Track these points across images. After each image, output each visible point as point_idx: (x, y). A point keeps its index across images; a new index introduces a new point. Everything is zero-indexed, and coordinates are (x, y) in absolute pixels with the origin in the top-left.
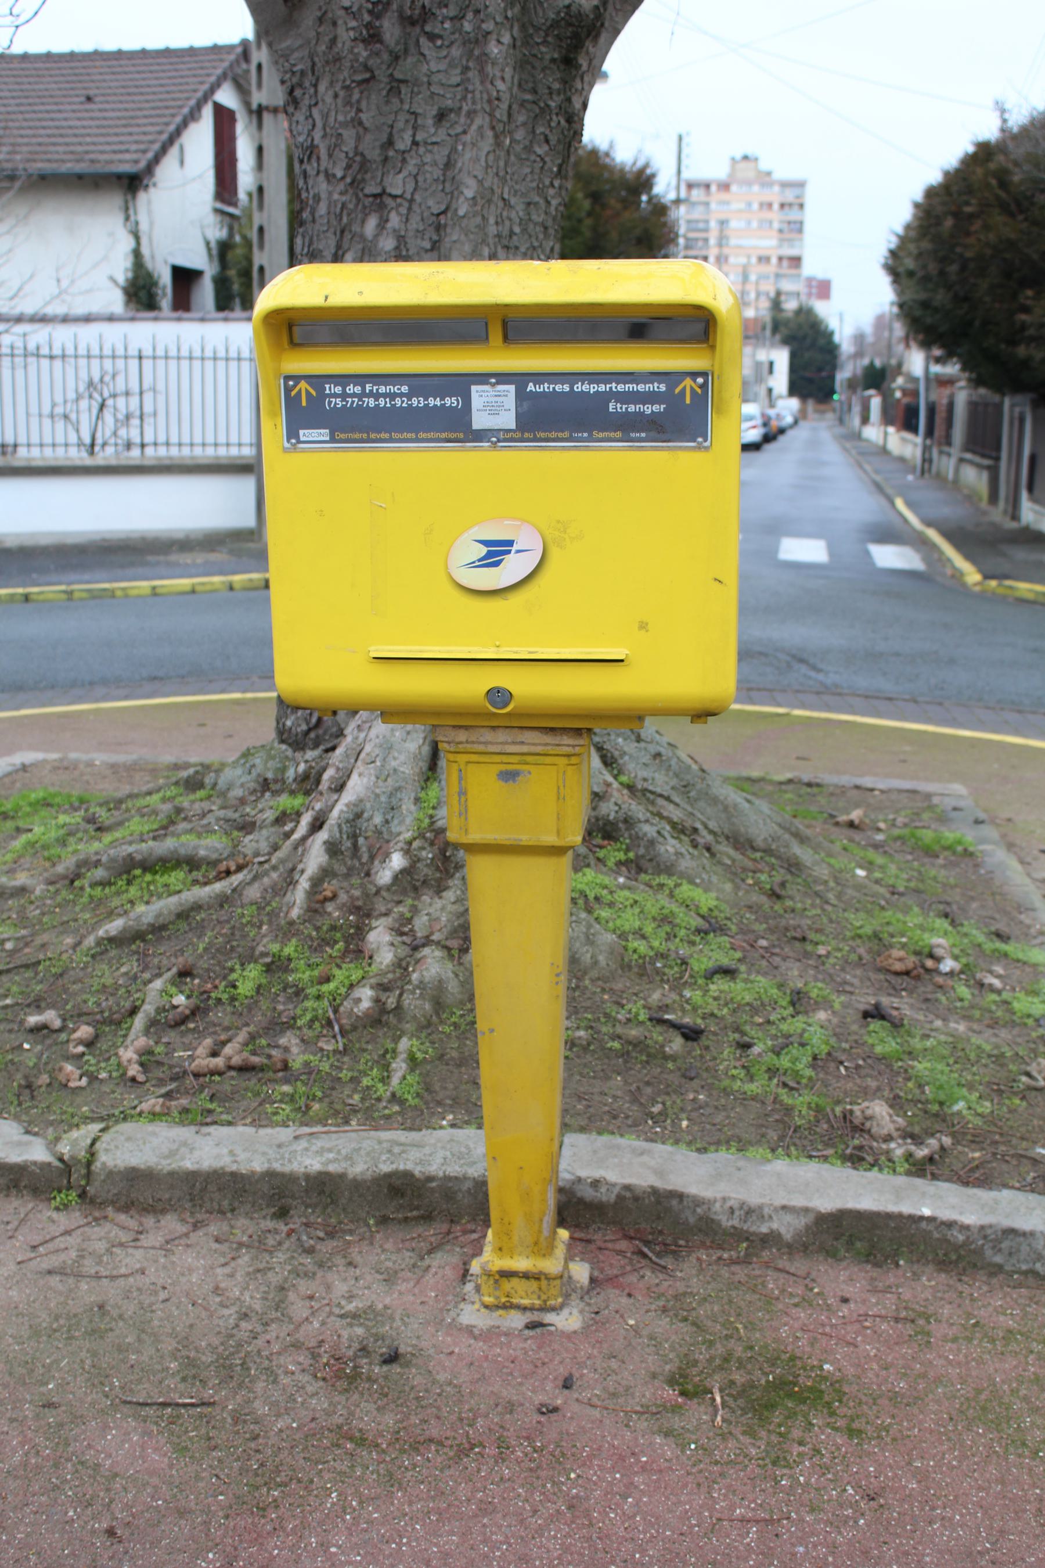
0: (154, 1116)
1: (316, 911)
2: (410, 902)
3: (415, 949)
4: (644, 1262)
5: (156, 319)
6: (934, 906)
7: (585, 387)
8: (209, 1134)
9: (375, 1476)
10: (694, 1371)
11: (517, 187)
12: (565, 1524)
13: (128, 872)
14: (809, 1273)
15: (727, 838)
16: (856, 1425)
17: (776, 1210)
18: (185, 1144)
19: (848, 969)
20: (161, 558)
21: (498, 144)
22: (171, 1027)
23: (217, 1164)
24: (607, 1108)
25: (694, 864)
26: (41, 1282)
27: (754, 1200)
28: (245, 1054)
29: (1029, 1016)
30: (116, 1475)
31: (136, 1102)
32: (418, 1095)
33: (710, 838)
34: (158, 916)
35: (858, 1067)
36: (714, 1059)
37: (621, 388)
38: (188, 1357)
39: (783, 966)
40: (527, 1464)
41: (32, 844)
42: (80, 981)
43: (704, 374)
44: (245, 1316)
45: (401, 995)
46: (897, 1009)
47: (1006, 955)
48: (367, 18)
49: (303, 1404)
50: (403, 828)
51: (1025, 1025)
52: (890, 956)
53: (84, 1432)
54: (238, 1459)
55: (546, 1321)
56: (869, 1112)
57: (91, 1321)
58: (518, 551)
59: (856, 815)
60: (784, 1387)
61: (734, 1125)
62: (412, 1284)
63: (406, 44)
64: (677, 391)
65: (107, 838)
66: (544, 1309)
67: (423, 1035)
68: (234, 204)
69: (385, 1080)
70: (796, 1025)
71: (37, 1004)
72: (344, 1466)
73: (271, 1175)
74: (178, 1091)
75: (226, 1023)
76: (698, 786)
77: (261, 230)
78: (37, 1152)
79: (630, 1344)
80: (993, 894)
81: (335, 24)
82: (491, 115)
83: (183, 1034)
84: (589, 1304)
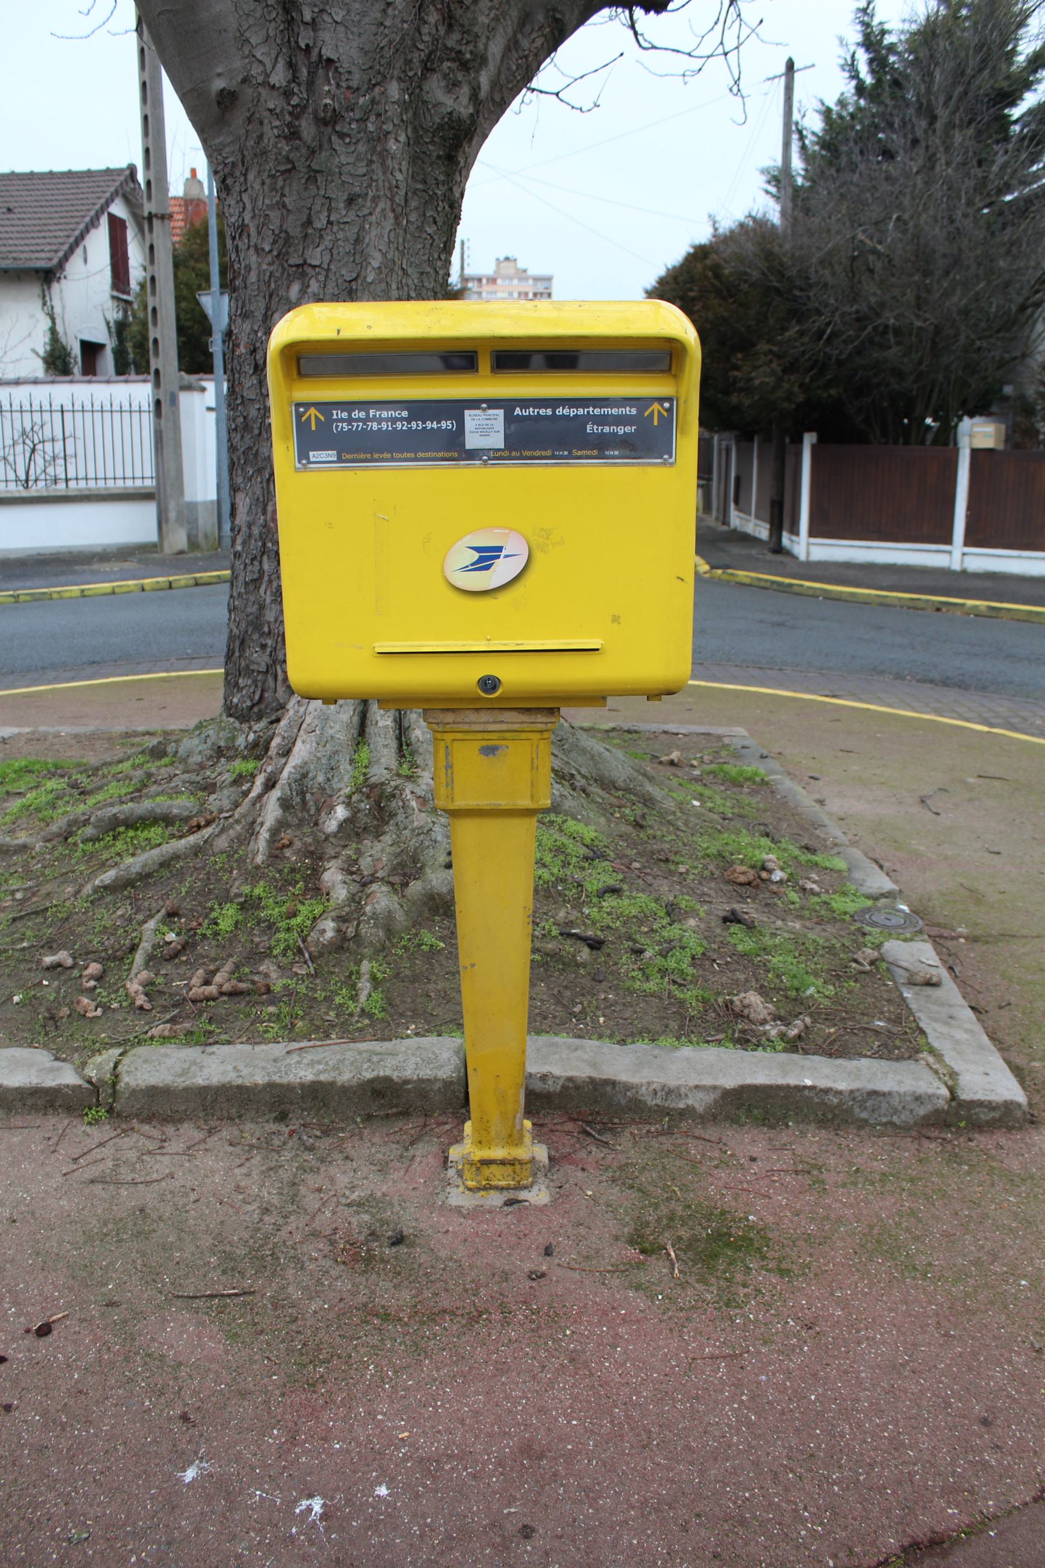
0: (164, 1039)
1: (276, 857)
2: (354, 845)
3: (364, 885)
4: (589, 1140)
5: (71, 382)
6: (756, 828)
7: (566, 411)
8: (213, 1053)
9: (403, 1347)
10: (648, 1231)
11: (412, 260)
12: (570, 1376)
13: (114, 829)
14: (720, 1139)
15: (596, 781)
16: (784, 1266)
17: (690, 1089)
18: (194, 1063)
19: (704, 883)
20: (86, 567)
21: (398, 223)
22: (166, 960)
23: (225, 1079)
24: (537, 1011)
25: (575, 803)
26: (87, 1191)
27: (673, 1083)
28: (234, 982)
29: (845, 913)
30: (180, 1364)
31: (147, 1028)
32: (384, 1010)
33: (583, 782)
34: (144, 866)
35: (727, 963)
36: (616, 964)
37: (597, 411)
38: (225, 1252)
39: (656, 883)
40: (528, 1326)
41: (27, 807)
42: (83, 923)
43: (670, 400)
44: (266, 1211)
45: (358, 925)
46: (747, 913)
47: (816, 864)
48: (288, 118)
49: (330, 1286)
50: (342, 785)
51: (844, 920)
52: (735, 871)
53: (146, 1326)
54: (283, 1341)
55: (521, 1198)
56: (746, 1002)
57: (135, 1224)
58: (506, 556)
59: (675, 755)
60: (720, 1237)
61: (641, 1018)
62: (402, 1172)
63: (320, 140)
64: (646, 414)
65: (91, 801)
66: (518, 1188)
67: (381, 958)
68: (128, 293)
69: (354, 998)
70: (673, 932)
71: (50, 946)
72: (375, 1340)
73: (271, 1086)
74: (180, 1017)
75: (213, 955)
76: (570, 740)
77: (154, 310)
78: (68, 1077)
79: (592, 1212)
80: (793, 815)
81: (261, 123)
82: (392, 200)
83: (177, 966)
84: (552, 1180)
